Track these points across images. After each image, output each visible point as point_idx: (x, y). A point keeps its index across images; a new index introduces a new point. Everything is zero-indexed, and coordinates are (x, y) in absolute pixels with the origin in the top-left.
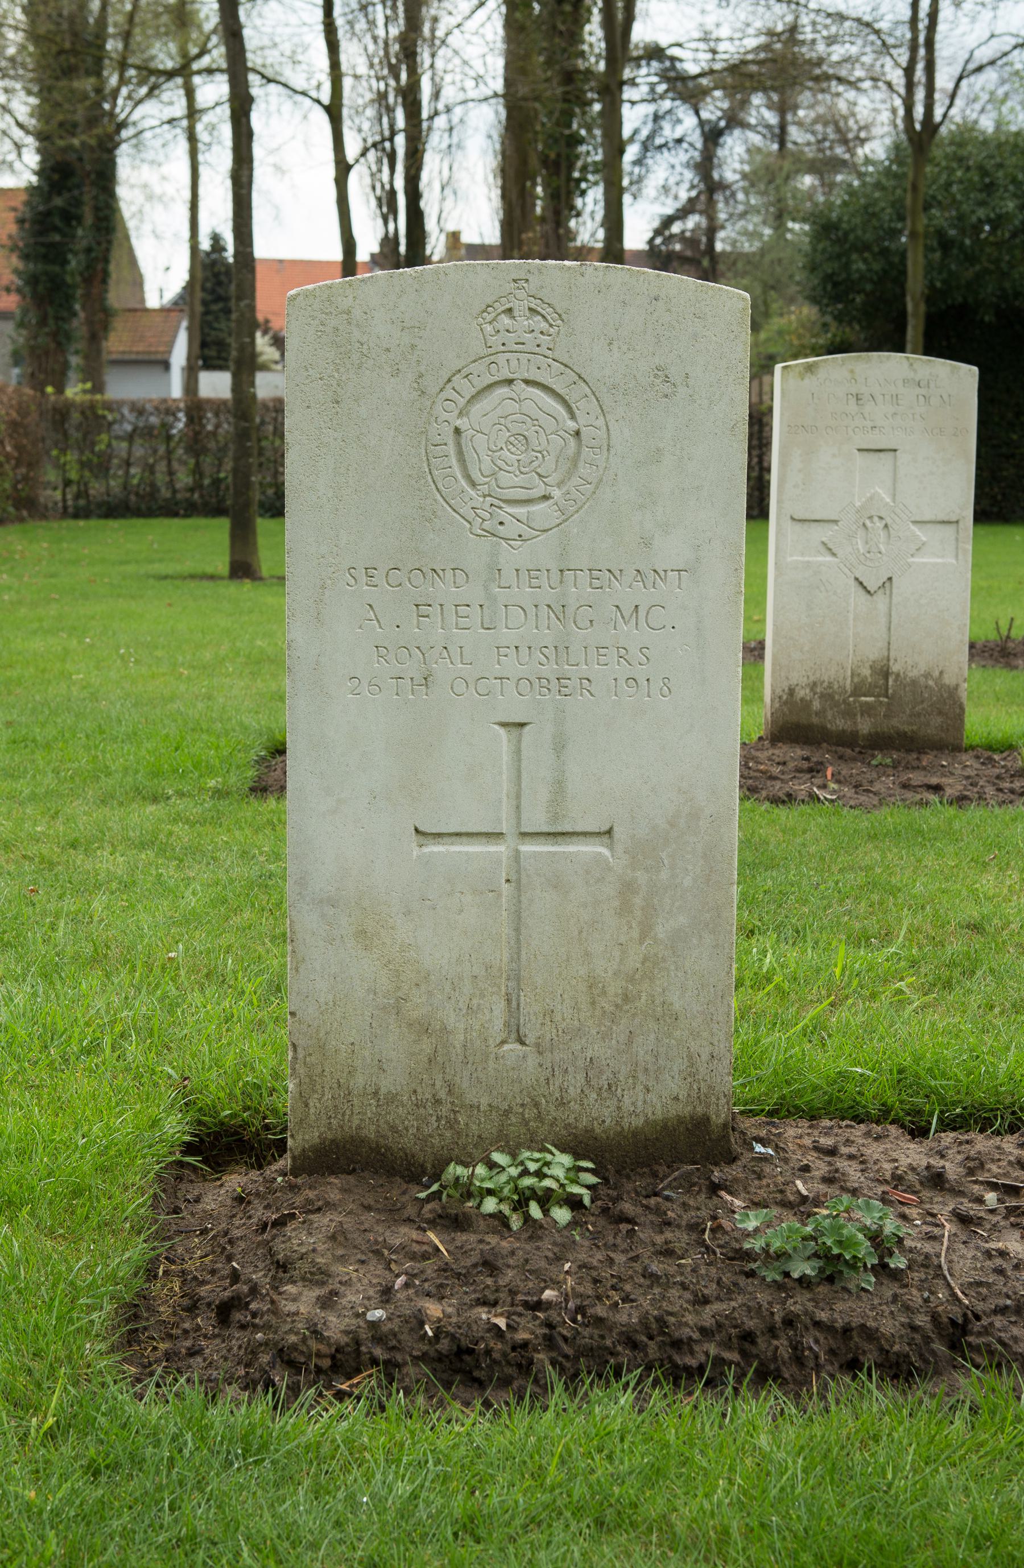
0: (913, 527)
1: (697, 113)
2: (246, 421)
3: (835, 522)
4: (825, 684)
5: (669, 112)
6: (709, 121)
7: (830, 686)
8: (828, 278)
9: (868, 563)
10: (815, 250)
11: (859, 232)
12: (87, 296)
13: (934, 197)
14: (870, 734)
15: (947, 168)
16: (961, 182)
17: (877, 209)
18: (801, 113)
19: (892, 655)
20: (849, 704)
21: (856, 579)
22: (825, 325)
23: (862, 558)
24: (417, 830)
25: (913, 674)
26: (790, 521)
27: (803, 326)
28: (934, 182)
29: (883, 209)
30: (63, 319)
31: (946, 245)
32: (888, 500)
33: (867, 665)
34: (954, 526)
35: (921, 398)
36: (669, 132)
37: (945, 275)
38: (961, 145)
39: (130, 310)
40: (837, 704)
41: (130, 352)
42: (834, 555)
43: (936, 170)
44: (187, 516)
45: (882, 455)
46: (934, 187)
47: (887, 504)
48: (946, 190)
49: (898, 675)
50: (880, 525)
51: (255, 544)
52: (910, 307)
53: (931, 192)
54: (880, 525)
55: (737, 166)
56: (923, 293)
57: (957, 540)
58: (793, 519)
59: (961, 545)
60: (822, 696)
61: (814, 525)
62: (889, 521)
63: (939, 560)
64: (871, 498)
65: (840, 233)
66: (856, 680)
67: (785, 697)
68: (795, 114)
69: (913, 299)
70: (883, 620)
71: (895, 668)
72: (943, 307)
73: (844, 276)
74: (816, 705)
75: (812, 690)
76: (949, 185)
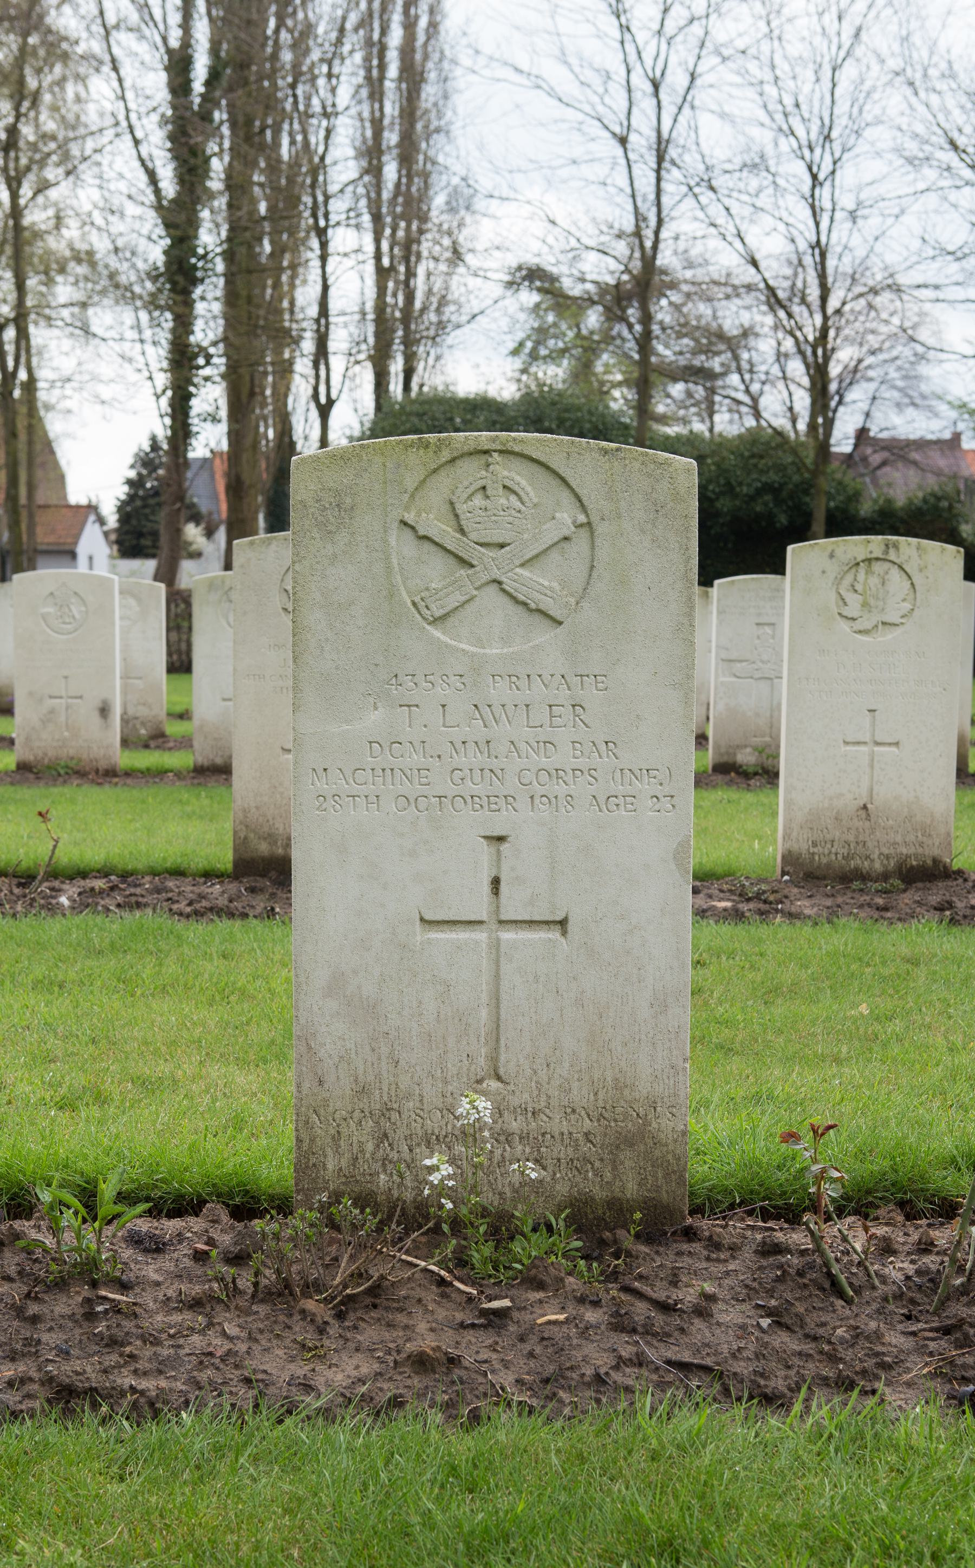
24: (422, 919)
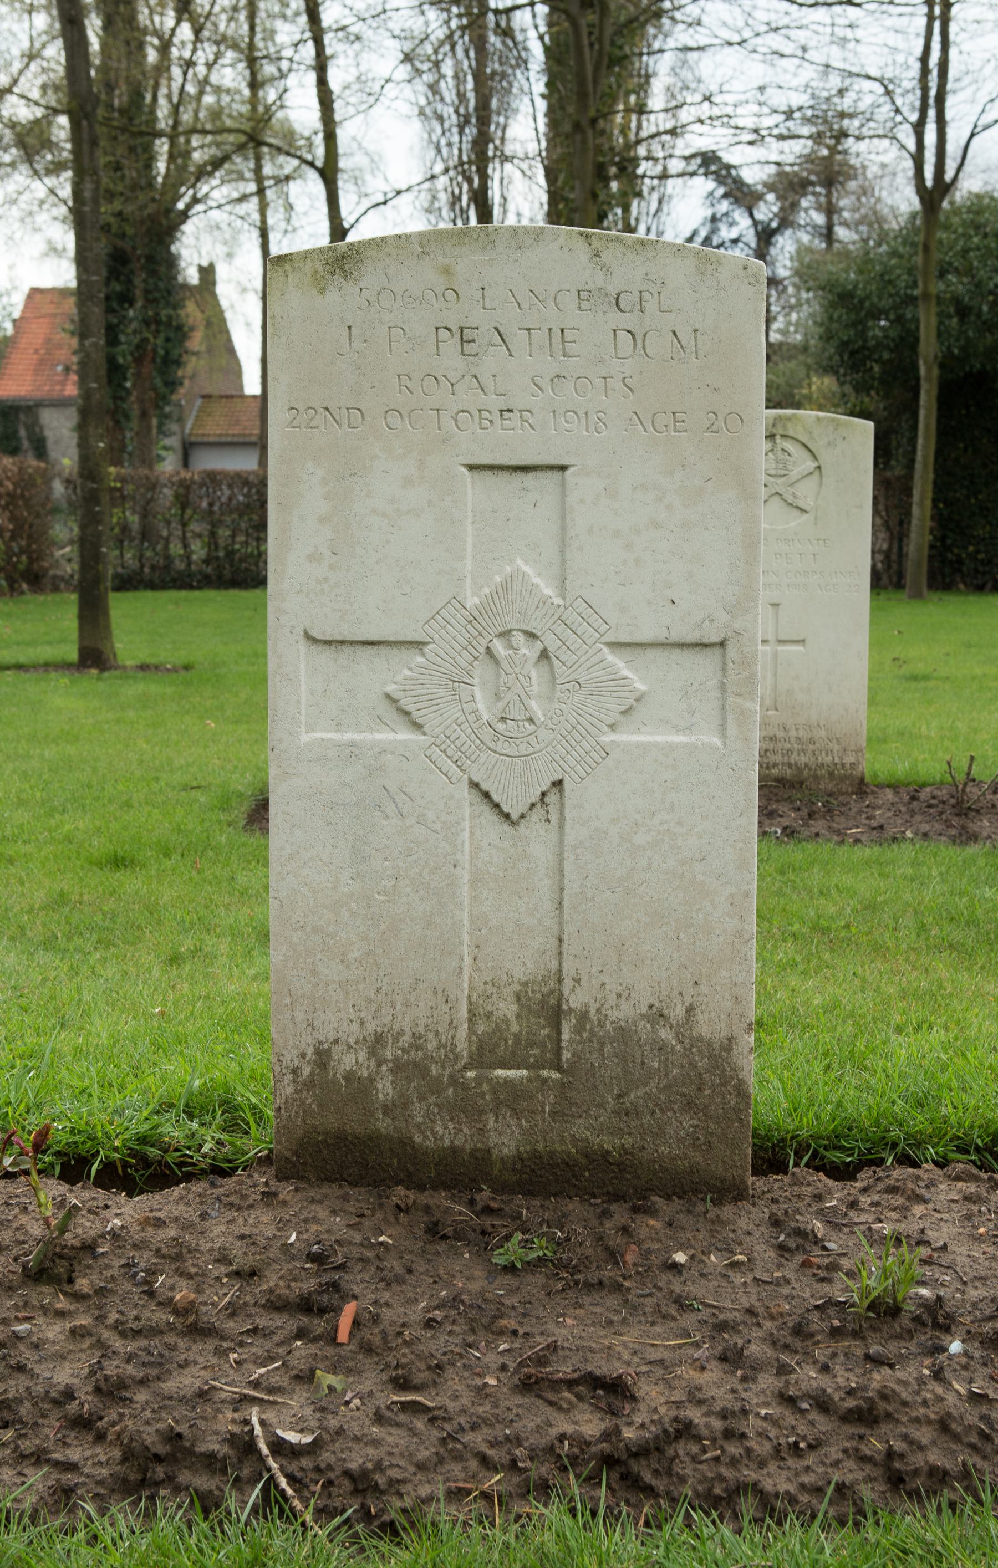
0: (610, 657)
1: (751, 215)
2: (94, 481)
3: (418, 645)
4: (406, 1039)
5: (726, 214)
6: (762, 222)
7: (417, 1042)
8: (844, 344)
9: (500, 746)
10: (831, 318)
11: (875, 299)
12: (138, 375)
13: (950, 264)
14: (519, 1157)
15: (964, 235)
16: (978, 249)
17: (893, 277)
18: (846, 214)
19: (569, 968)
20: (465, 1087)
21: (475, 785)
22: (844, 395)
23: (487, 734)
25: (622, 1013)
26: (303, 646)
27: (824, 397)
28: (951, 249)
29: (899, 276)
30: (121, 398)
31: (963, 311)
32: (548, 591)
33: (508, 992)
34: (713, 657)
35: (623, 337)
36: (726, 233)
37: (962, 342)
38: (979, 212)
39: (227, 397)
40: (436, 1087)
41: (227, 435)
42: (417, 726)
43: (953, 236)
44: (199, 588)
45: (529, 479)
46: (951, 254)
47: (544, 601)
48: (963, 257)
49: (583, 1016)
50: (529, 651)
51: (107, 627)
52: (923, 371)
53: (947, 259)
54: (529, 651)
55: (788, 263)
56: (936, 357)
57: (723, 687)
58: (311, 639)
59: (731, 700)
60: (398, 1068)
61: (362, 652)
62: (552, 643)
63: (681, 739)
64: (505, 587)
65: (856, 301)
66: (481, 1028)
67: (306, 1071)
68: (841, 216)
69: (925, 362)
70: (545, 885)
71: (576, 999)
72: (961, 374)
73: (860, 343)
74: (385, 1089)
75: (372, 1053)
76: (965, 251)
